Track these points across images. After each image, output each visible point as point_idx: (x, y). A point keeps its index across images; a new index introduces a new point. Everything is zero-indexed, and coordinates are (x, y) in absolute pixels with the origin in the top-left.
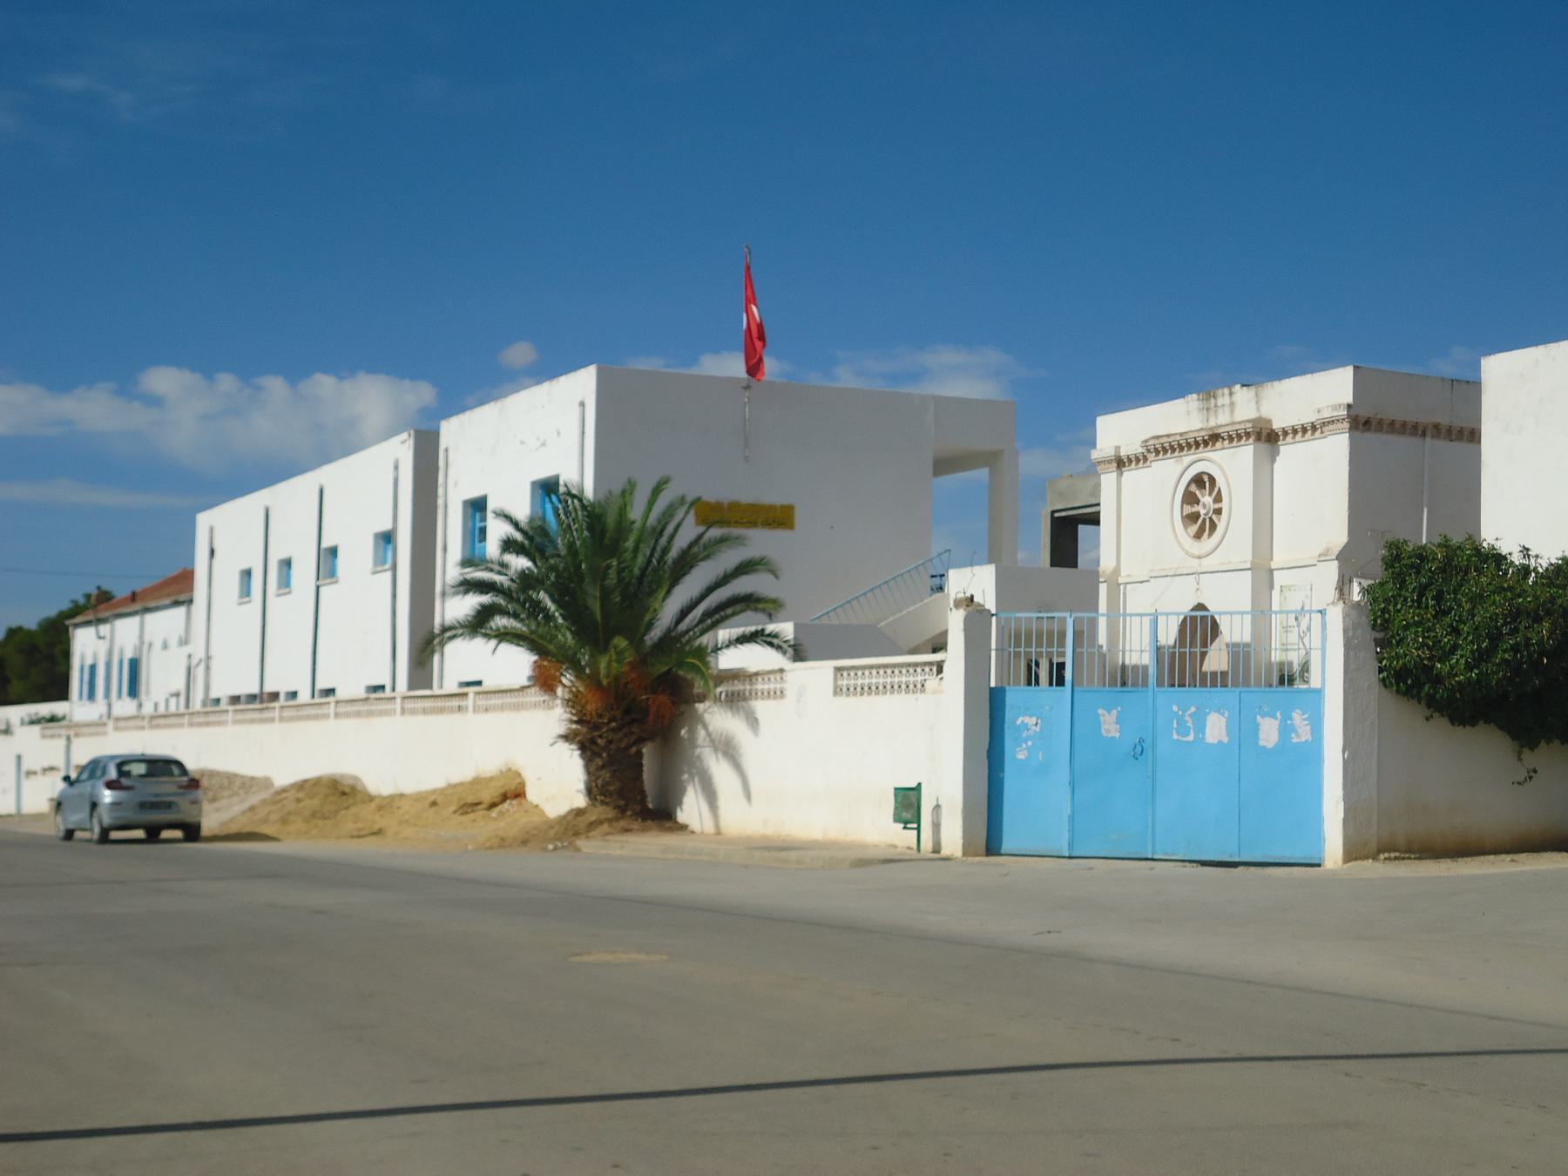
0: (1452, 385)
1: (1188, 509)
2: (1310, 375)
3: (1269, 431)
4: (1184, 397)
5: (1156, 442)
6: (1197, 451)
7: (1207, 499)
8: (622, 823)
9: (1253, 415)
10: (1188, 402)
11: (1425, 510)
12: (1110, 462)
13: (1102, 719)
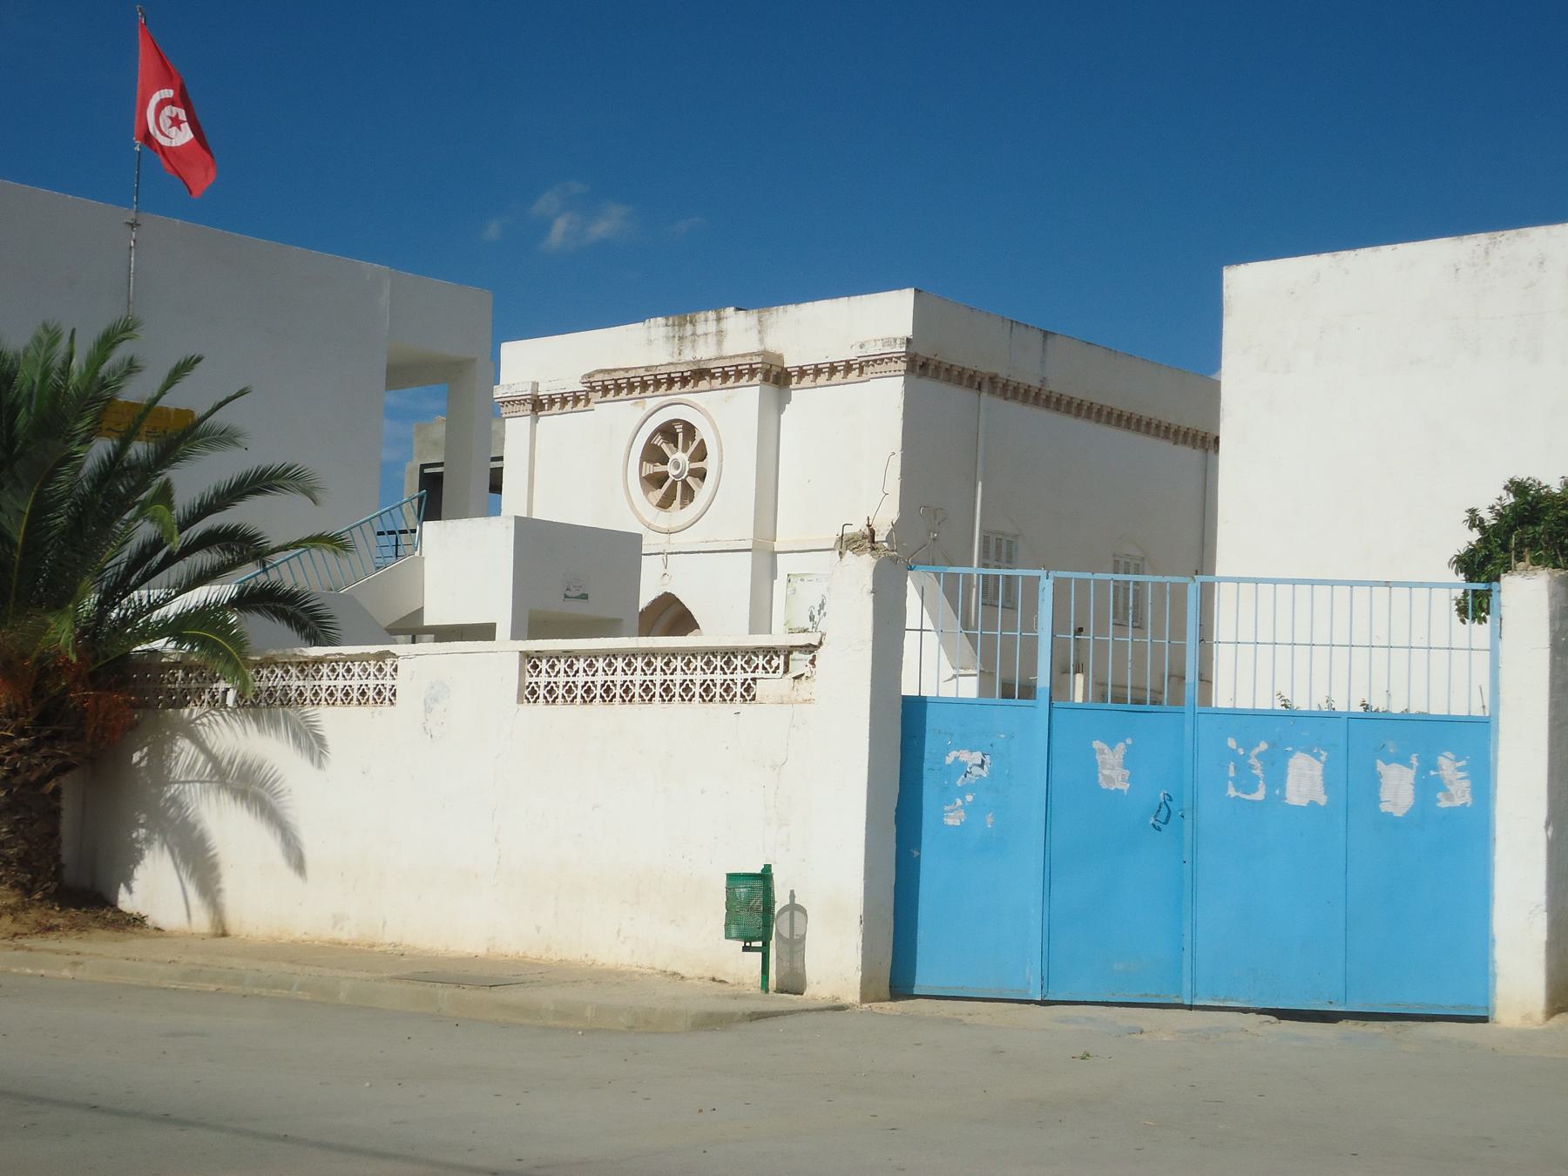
0: (1012, 327)
1: (649, 469)
2: (811, 303)
3: (780, 370)
4: (644, 321)
5: (607, 377)
6: (669, 392)
7: (680, 458)
8: (34, 914)
9: (755, 347)
10: (649, 327)
11: (980, 484)
12: (521, 402)
13: (1098, 757)
